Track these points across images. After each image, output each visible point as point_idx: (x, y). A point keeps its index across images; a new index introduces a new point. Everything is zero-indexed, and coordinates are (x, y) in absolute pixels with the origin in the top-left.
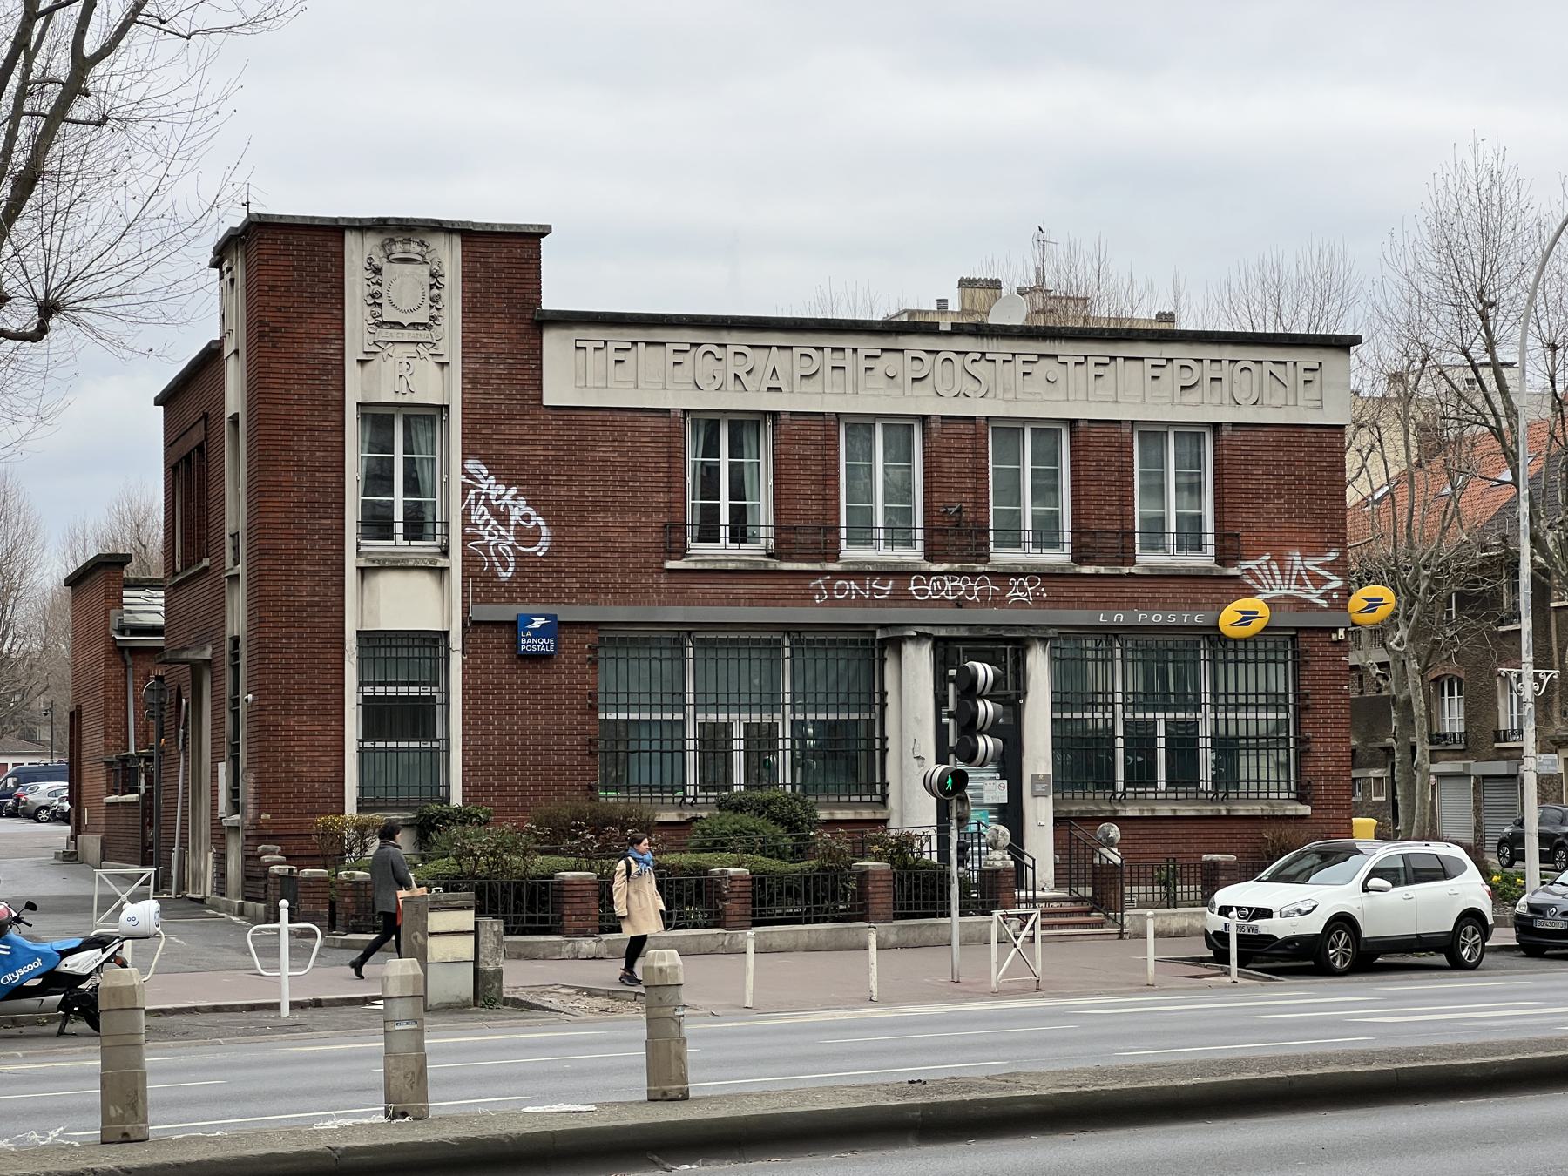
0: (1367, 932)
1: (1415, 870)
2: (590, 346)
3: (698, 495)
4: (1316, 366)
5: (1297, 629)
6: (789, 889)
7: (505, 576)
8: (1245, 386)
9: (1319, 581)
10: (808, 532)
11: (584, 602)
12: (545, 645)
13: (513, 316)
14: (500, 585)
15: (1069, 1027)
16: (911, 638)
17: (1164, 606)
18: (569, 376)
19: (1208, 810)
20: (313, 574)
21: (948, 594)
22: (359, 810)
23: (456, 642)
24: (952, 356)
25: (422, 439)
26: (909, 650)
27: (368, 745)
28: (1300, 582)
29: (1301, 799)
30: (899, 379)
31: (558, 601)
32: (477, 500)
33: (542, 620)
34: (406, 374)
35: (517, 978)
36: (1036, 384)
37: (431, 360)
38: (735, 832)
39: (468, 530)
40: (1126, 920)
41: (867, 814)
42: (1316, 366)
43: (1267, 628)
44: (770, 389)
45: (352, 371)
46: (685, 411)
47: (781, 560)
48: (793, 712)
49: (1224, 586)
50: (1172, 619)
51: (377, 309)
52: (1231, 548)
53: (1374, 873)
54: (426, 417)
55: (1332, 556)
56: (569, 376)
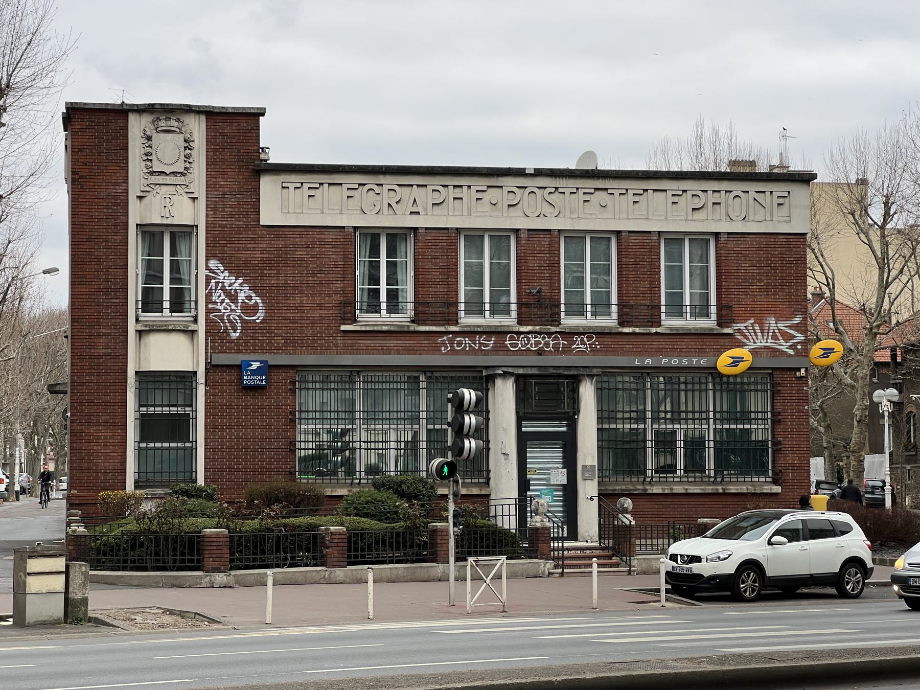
0: (769, 573)
1: (810, 530)
2: (292, 186)
3: (366, 281)
4: (786, 194)
5: (773, 369)
6: (377, 543)
7: (235, 335)
8: (737, 208)
9: (788, 337)
10: (436, 306)
11: (286, 352)
12: (260, 380)
13: (241, 167)
14: (232, 341)
15: (378, 645)
16: (500, 375)
17: (680, 353)
18: (276, 205)
19: (709, 489)
20: (106, 334)
21: (532, 347)
22: (136, 487)
23: (201, 378)
24: (536, 190)
25: (182, 247)
26: (499, 382)
27: (144, 445)
28: (774, 337)
29: (775, 482)
30: (499, 205)
31: (270, 351)
32: (216, 286)
34: (168, 205)
35: (100, 601)
36: (593, 208)
37: (186, 196)
38: (367, 503)
39: (210, 306)
40: (634, 562)
41: (475, 491)
42: (786, 194)
43: (750, 368)
44: (411, 213)
45: (134, 205)
46: (355, 228)
47: (419, 324)
48: (715, 423)
49: (722, 341)
50: (685, 362)
51: (149, 163)
52: (727, 315)
53: (778, 532)
54: (182, 234)
55: (797, 320)
56: (276, 205)
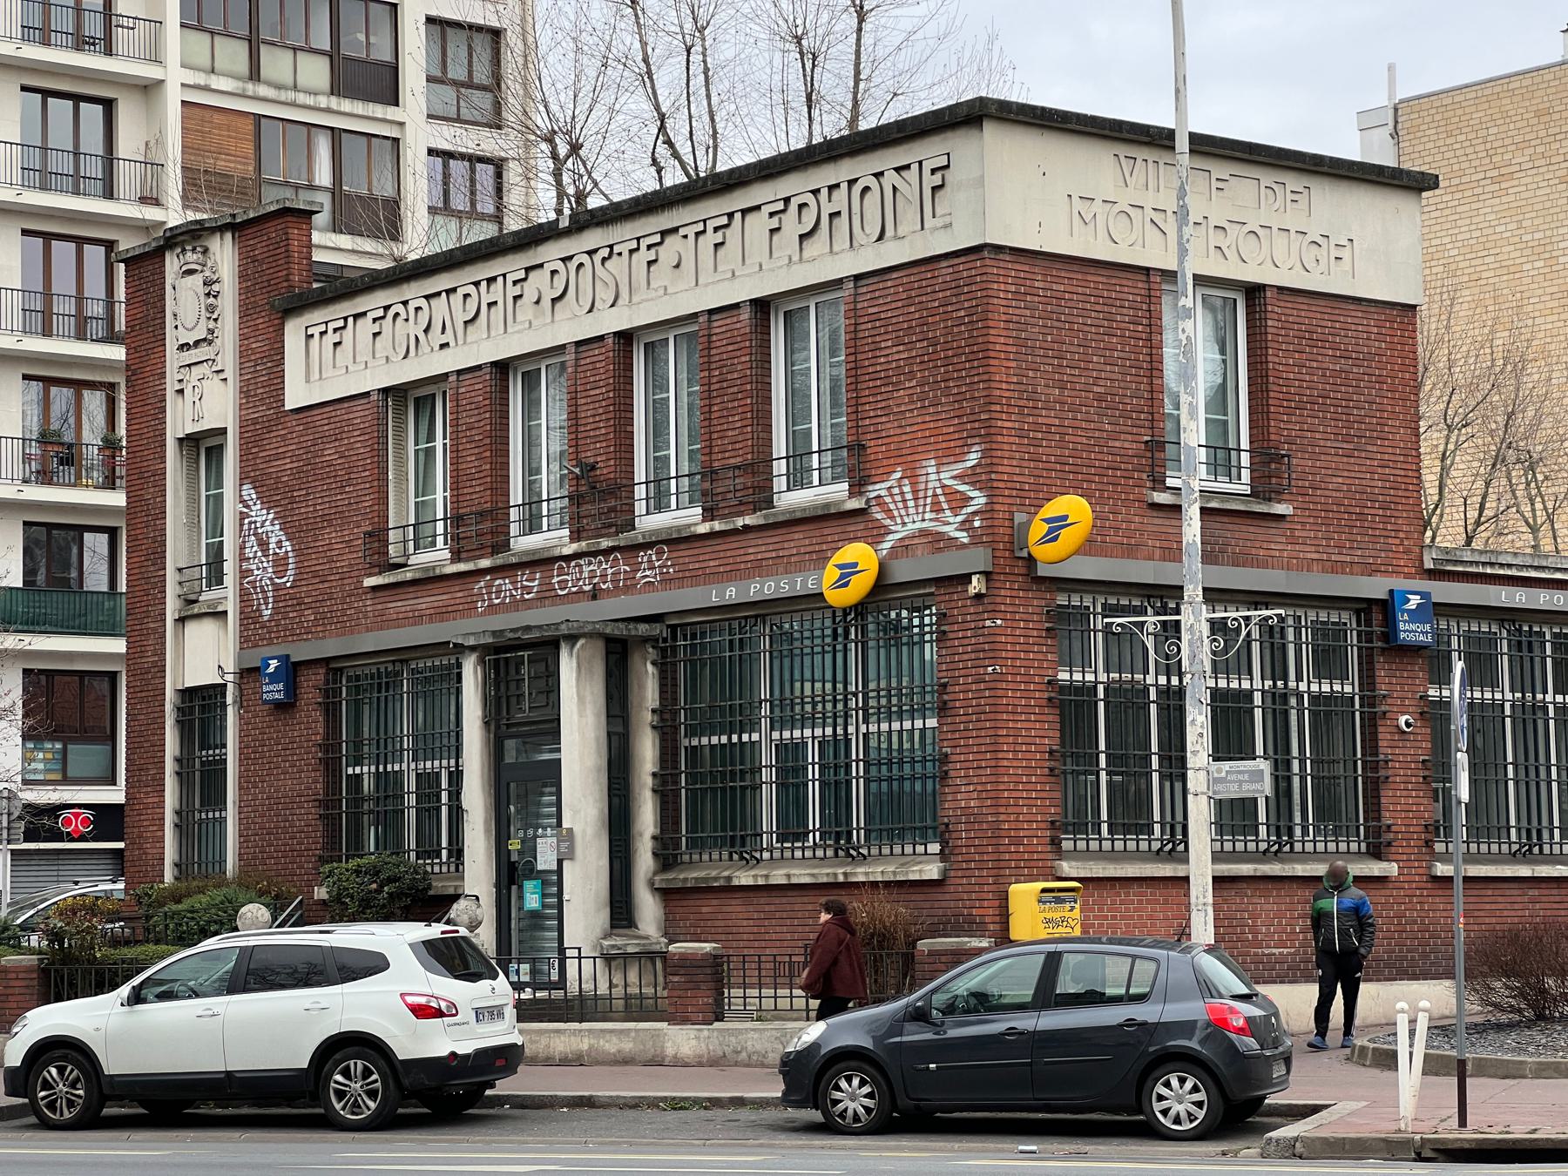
33: (274, 663)
48: (866, 721)
55: (973, 458)
